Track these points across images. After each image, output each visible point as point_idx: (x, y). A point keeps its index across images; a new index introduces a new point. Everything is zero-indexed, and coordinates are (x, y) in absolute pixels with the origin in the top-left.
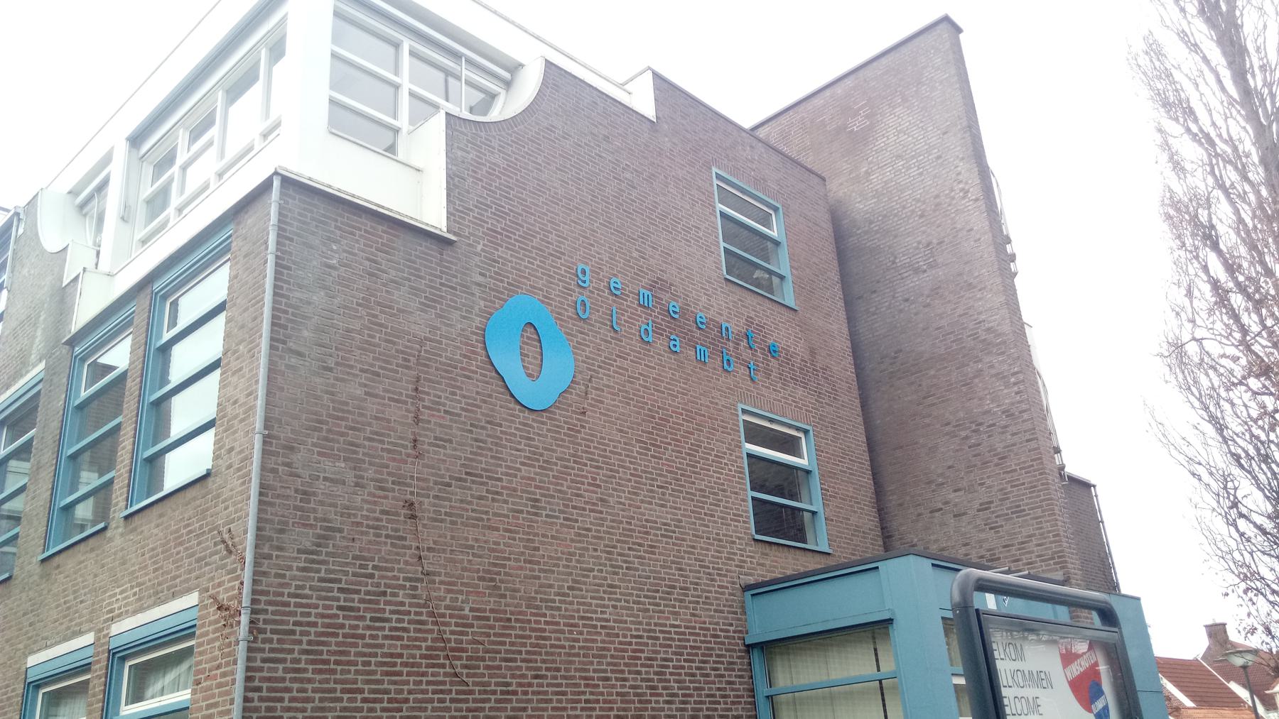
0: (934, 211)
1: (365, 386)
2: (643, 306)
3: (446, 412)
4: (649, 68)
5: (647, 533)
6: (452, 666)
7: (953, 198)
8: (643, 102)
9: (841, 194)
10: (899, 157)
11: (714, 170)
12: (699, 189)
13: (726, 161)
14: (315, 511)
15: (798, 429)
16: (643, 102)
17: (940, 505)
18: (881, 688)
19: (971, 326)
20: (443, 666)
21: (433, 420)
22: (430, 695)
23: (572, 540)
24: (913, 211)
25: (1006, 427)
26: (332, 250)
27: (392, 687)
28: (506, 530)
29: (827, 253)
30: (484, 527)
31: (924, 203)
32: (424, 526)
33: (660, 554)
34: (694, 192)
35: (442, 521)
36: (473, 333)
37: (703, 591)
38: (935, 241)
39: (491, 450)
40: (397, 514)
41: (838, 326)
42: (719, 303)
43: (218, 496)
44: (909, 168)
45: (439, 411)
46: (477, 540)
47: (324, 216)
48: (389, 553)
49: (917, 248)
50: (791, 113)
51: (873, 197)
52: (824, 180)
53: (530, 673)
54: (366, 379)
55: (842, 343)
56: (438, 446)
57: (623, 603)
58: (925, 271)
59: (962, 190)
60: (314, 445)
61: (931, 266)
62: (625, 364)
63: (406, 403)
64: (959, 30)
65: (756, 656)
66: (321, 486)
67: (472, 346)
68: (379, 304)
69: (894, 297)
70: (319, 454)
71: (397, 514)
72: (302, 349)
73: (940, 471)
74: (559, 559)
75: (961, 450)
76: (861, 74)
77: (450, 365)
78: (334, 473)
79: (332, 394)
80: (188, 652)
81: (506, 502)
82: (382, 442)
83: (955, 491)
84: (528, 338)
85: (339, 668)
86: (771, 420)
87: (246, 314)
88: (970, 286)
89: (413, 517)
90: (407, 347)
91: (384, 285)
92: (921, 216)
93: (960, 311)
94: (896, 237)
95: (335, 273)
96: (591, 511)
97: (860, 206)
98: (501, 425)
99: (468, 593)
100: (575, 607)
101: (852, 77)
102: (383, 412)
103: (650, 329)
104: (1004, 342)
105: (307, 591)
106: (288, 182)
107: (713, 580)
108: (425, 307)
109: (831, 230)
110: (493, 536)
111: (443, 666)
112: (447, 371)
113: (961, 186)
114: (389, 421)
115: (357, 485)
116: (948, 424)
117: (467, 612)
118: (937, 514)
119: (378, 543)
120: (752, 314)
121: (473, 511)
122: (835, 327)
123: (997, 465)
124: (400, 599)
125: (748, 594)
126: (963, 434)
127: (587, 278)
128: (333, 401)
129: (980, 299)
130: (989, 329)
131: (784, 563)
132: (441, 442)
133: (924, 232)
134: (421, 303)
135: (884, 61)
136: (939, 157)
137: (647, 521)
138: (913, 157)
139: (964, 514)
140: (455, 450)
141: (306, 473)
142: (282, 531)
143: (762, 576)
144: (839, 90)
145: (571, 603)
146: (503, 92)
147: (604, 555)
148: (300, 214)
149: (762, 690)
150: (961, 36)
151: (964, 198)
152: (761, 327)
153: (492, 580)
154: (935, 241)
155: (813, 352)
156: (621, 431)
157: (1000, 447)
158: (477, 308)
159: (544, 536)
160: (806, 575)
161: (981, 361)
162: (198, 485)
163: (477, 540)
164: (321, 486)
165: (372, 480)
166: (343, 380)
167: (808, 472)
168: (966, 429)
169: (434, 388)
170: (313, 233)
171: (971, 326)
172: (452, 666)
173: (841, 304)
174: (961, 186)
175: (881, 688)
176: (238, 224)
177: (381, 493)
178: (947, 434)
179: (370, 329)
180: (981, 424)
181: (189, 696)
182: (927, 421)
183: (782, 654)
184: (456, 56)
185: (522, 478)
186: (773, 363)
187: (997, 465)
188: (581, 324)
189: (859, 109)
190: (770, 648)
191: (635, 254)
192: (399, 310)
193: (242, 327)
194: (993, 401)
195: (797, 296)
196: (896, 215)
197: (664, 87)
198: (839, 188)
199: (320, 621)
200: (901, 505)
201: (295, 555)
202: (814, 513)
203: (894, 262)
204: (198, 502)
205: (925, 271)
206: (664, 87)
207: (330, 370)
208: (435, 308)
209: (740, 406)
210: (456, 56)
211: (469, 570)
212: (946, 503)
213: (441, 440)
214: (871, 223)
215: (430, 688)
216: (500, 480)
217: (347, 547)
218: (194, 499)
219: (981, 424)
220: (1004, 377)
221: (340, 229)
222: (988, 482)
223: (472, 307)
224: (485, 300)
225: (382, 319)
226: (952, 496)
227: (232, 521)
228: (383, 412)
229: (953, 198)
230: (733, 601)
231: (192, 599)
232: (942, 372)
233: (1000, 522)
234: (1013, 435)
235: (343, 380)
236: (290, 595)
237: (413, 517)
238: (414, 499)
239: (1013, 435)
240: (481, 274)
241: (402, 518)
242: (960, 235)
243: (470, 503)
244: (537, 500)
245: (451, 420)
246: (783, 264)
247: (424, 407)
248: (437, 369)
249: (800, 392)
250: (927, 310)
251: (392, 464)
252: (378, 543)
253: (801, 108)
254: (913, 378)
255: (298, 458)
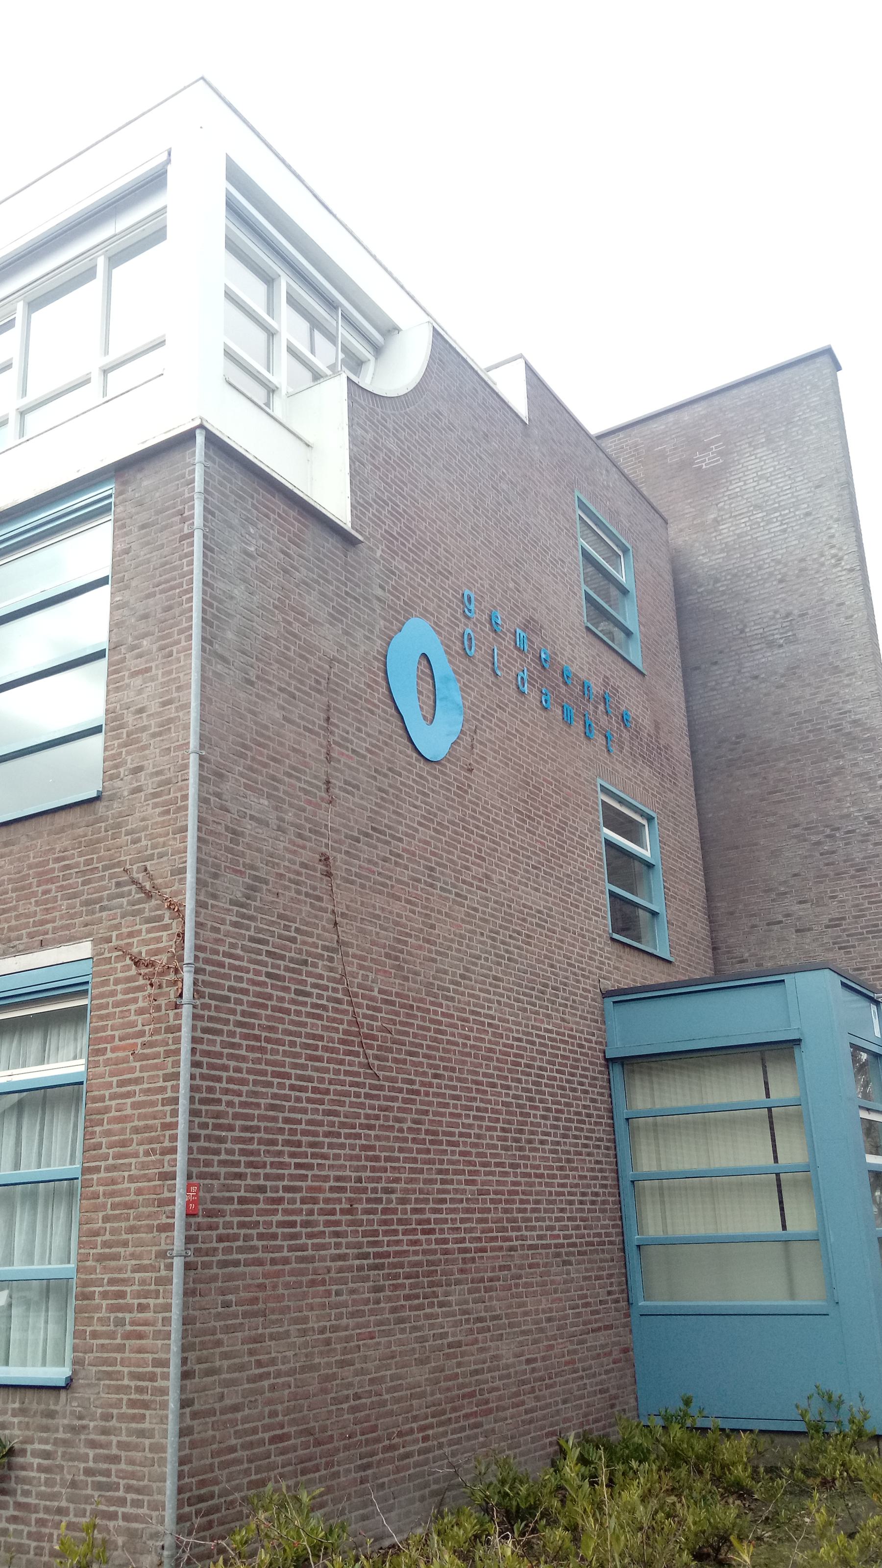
0: (798, 577)
1: (283, 708)
2: (519, 649)
3: (354, 751)
4: (521, 356)
5: (524, 920)
6: (366, 1056)
7: (823, 565)
8: (518, 399)
9: (680, 542)
10: (757, 507)
11: (577, 493)
12: (564, 514)
13: (586, 485)
14: (243, 855)
15: (643, 814)
16: (518, 399)
17: (780, 918)
18: (770, 1117)
19: (834, 715)
20: (357, 1054)
21: (343, 760)
22: (347, 1088)
23: (463, 921)
24: (771, 574)
25: (868, 835)
26: (250, 534)
27: (315, 1074)
28: (408, 902)
29: (668, 612)
30: (388, 894)
31: (786, 565)
32: (338, 886)
33: (536, 946)
34: (560, 517)
35: (353, 883)
36: (375, 658)
37: (571, 993)
38: (796, 612)
39: (392, 803)
40: (315, 869)
41: (676, 699)
42: (580, 657)
43: (119, 826)
44: (769, 522)
45: (347, 749)
46: (383, 909)
47: (241, 489)
48: (309, 915)
49: (773, 618)
50: (621, 435)
51: (722, 551)
52: (666, 522)
53: (431, 1072)
54: (285, 700)
55: (680, 721)
56: (348, 792)
57: (505, 1000)
58: (781, 646)
59: (834, 556)
60: (241, 774)
61: (788, 641)
62: (505, 716)
63: (317, 734)
64: (838, 367)
65: (616, 1071)
66: (249, 826)
67: (374, 673)
68: (292, 609)
69: (739, 672)
70: (246, 786)
71: (315, 869)
72: (226, 654)
73: (782, 879)
74: (452, 941)
75: (811, 856)
76: (716, 400)
77: (355, 695)
78: (259, 812)
79: (254, 713)
80: (79, 1015)
81: (406, 867)
82: (299, 779)
83: (800, 902)
84: (422, 671)
85: (269, 1046)
86: (621, 801)
87: (151, 601)
88: (836, 670)
89: (329, 874)
90: (318, 667)
91: (297, 586)
92: (781, 581)
93: (821, 697)
94: (747, 601)
95: (253, 564)
96: (479, 888)
97: (705, 560)
98: (400, 775)
99: (377, 971)
100: (467, 999)
101: (704, 404)
102: (299, 743)
103: (525, 677)
104: (872, 739)
105: (239, 952)
106: (215, 442)
107: (578, 981)
108: (334, 619)
109: (671, 584)
110: (397, 907)
111: (357, 1054)
112: (352, 701)
113: (833, 551)
114: (304, 755)
115: (279, 829)
116: (796, 826)
117: (376, 993)
118: (776, 927)
119: (299, 901)
120: (608, 674)
121: (379, 874)
122: (675, 700)
123: (853, 877)
124: (319, 971)
125: (609, 1001)
126: (814, 838)
127: (472, 607)
128: (256, 723)
129: (848, 686)
130: (855, 721)
131: (635, 972)
132: (352, 786)
133: (784, 600)
134: (330, 614)
135: (746, 389)
136: (808, 514)
137: (524, 906)
138: (776, 510)
139: (809, 929)
140: (362, 798)
141: (234, 808)
142: (215, 876)
143: (619, 982)
144: (685, 416)
145: (463, 994)
146: (372, 359)
147: (489, 941)
148: (221, 484)
149: (622, 1112)
150: (839, 373)
151: (835, 566)
152: (616, 689)
153: (397, 958)
154: (796, 612)
155: (657, 726)
156: (502, 796)
157: (858, 857)
158: (377, 627)
159: (440, 912)
160: (663, 986)
161: (842, 757)
162: (78, 810)
163: (383, 909)
164: (249, 826)
165: (292, 824)
166: (263, 698)
167: (650, 866)
168: (818, 833)
169: (343, 721)
170: (233, 510)
171: (834, 715)
172: (366, 1056)
173: (679, 673)
174: (833, 551)
175: (770, 1117)
176: (125, 483)
177: (300, 841)
178: (795, 837)
179: (286, 639)
180: (838, 829)
181: (82, 1068)
182: (771, 819)
183: (641, 1072)
184: (331, 305)
185: (420, 841)
186: (626, 735)
187: (853, 877)
188: (466, 662)
189: (712, 443)
190: (630, 1064)
191: (511, 585)
192: (310, 619)
193: (145, 617)
194: (854, 804)
195: (644, 657)
196: (748, 576)
197: (536, 384)
198: (680, 534)
199: (251, 988)
200: (732, 913)
201: (227, 906)
202: (654, 914)
203: (742, 631)
204: (80, 831)
205: (781, 646)
206: (536, 384)
207: (252, 684)
208: (341, 622)
209: (600, 781)
210: (331, 305)
211: (377, 945)
212: (788, 915)
213: (350, 784)
214: (717, 581)
215: (348, 1079)
216: (400, 840)
217: (272, 902)
218: (72, 826)
219: (838, 829)
220: (870, 778)
221: (257, 509)
222: (841, 896)
223: (373, 626)
224: (384, 619)
225: (296, 627)
226: (796, 907)
227: (151, 858)
228: (299, 743)
229: (823, 565)
230: (595, 1007)
231: (84, 949)
232: (794, 765)
233: (853, 941)
234: (876, 844)
235: (263, 698)
236: (862, 928)
237: (329, 874)
238: (329, 852)
239: (876, 844)
240: (381, 587)
241: (318, 874)
242: (828, 608)
243: (376, 864)
244: (432, 869)
245: (358, 762)
246: (630, 617)
247: (335, 743)
248: (345, 698)
249: (647, 772)
250: (779, 691)
251: (309, 808)
252: (299, 901)
253: (636, 430)
254: (757, 769)
255: (227, 787)
